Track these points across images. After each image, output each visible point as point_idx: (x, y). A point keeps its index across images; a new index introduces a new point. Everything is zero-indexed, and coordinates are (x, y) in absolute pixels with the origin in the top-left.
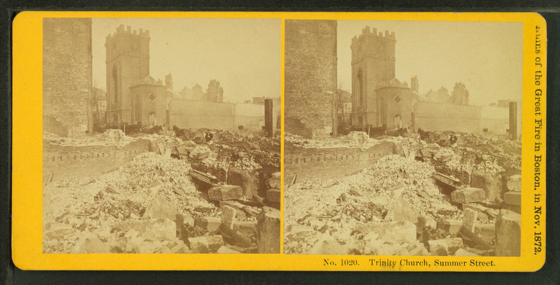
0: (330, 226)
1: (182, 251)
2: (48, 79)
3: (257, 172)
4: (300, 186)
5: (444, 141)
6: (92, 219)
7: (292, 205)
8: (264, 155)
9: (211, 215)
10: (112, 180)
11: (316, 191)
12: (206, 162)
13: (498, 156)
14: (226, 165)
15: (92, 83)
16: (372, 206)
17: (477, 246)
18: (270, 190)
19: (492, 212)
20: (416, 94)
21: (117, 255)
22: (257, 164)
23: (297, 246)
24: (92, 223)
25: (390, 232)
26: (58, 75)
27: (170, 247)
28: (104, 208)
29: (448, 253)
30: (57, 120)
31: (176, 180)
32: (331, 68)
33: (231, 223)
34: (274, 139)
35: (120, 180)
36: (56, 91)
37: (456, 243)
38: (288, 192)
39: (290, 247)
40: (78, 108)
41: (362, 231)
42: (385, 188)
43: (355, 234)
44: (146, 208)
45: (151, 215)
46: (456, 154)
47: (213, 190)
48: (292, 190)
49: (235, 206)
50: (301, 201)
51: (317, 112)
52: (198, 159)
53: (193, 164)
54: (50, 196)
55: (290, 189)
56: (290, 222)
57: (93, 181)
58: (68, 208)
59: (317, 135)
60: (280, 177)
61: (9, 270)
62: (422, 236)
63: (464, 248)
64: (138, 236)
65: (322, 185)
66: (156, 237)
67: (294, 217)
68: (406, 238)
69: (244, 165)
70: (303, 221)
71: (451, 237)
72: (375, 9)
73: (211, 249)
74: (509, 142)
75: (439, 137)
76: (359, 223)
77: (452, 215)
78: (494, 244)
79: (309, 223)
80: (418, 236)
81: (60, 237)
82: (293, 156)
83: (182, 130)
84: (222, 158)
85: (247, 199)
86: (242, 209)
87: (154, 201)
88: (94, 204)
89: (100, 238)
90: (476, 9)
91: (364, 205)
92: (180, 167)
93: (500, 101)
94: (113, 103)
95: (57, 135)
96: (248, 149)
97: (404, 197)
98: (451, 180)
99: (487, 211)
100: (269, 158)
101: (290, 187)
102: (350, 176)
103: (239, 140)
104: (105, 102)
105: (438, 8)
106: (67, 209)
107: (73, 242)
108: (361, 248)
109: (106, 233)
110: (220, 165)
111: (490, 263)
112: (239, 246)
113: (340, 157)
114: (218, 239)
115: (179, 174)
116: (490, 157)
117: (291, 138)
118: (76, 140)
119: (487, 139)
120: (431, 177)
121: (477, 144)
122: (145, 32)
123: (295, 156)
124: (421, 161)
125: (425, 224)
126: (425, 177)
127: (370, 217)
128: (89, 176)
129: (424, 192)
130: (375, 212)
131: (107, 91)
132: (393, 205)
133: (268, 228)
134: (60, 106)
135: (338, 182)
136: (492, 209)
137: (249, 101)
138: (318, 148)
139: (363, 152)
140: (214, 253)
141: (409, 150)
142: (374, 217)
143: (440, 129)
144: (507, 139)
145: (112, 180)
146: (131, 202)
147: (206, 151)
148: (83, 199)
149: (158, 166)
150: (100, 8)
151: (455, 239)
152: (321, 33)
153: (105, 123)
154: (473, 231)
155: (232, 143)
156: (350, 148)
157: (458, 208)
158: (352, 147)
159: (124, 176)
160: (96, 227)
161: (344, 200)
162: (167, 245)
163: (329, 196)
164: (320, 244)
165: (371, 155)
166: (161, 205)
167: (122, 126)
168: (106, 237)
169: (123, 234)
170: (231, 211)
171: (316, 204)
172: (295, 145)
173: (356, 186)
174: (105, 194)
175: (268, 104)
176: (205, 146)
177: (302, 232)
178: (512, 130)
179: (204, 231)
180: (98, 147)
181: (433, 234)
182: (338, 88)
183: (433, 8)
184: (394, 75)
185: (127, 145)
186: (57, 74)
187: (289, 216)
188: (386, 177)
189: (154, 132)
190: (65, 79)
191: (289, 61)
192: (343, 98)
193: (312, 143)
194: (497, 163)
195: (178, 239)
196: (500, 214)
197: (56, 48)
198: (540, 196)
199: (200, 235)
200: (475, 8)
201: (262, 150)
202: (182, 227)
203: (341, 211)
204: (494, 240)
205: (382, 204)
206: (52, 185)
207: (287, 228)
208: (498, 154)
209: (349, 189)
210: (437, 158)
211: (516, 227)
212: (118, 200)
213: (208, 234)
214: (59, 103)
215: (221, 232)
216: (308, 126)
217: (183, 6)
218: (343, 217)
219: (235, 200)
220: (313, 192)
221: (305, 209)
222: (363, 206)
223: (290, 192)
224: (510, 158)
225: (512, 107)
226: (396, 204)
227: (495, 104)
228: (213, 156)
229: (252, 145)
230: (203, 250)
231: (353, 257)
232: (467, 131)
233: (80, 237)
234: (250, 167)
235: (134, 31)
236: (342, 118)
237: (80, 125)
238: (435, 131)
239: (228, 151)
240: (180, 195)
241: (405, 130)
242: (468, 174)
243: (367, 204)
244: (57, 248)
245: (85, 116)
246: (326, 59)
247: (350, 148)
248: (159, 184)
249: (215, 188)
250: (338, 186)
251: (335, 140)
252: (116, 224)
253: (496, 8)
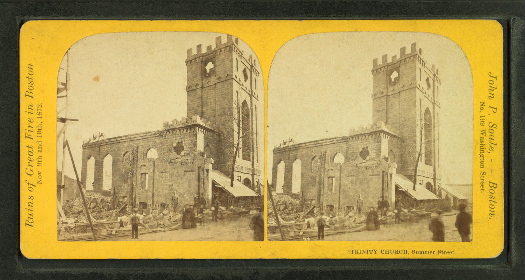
61: (16, 258)
105: (394, 15)
111: (483, 189)
150: (97, 16)
198: (28, 111)
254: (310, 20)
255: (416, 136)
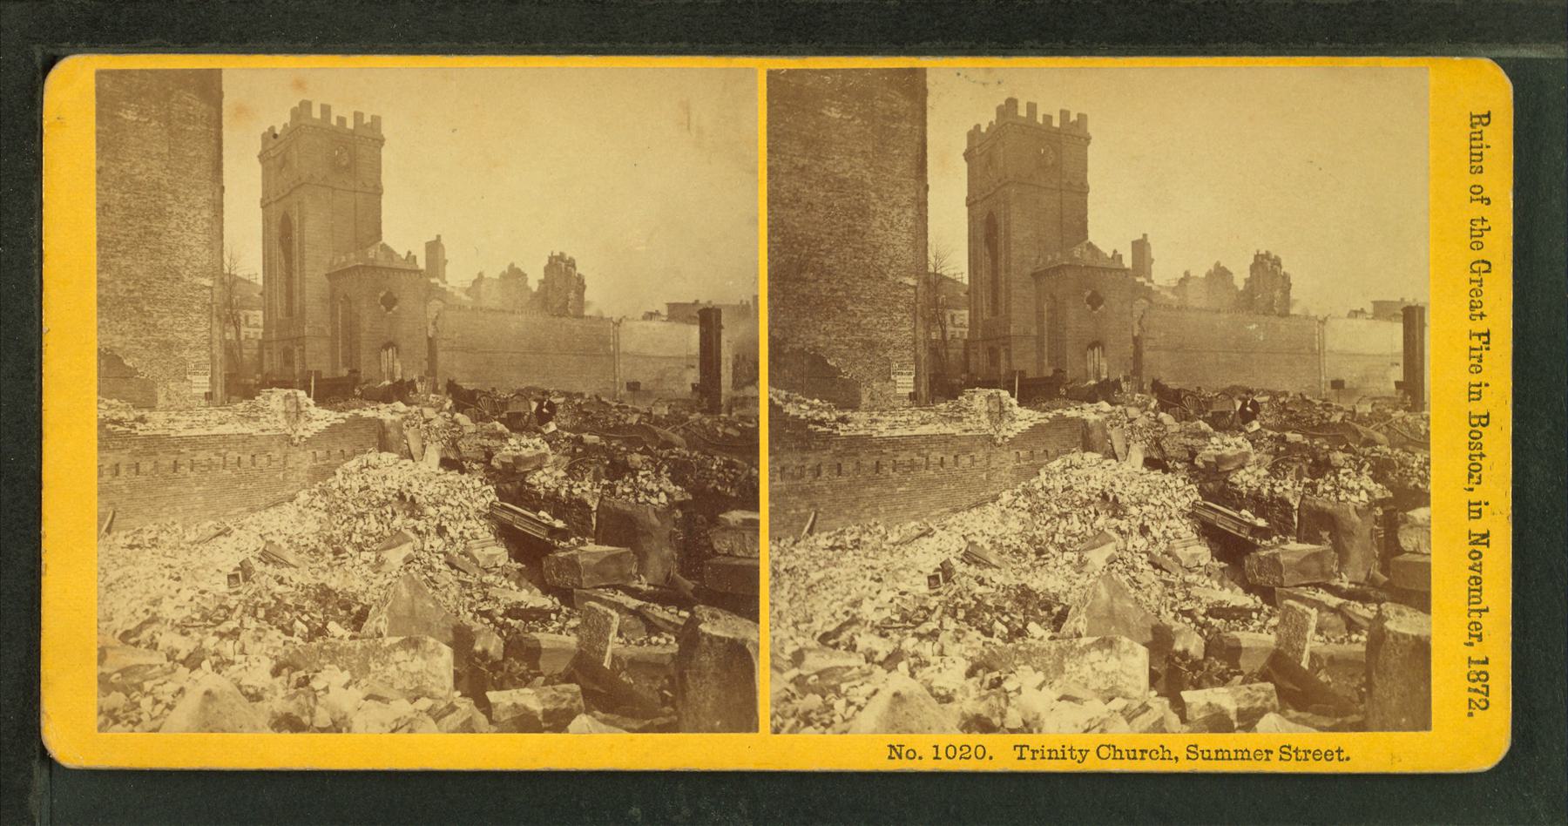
0: (213, 649)
1: (468, 727)
2: (806, 247)
3: (1378, 509)
4: (826, 542)
5: (1224, 414)
6: (222, 635)
7: (803, 593)
8: (1399, 461)
9: (551, 629)
10: (278, 530)
11: (168, 553)
12: (1239, 481)
13: (1374, 455)
14: (592, 488)
15: (222, 260)
16: (1025, 596)
17: (1315, 705)
18: (1400, 558)
19: (1362, 611)
20: (441, 285)
21: (287, 736)
22: (1379, 486)
23: (820, 707)
24: (221, 647)
25: (380, 668)
26: (128, 239)
27: (437, 716)
28: (256, 607)
29: (1236, 725)
30: (125, 361)
31: (455, 529)
32: (206, 216)
33: (1304, 650)
34: (725, 418)
35: (300, 529)
36: (828, 281)
37: (1258, 699)
38: (793, 558)
39: (800, 711)
40: (183, 331)
41: (997, 665)
42: (1062, 545)
43: (980, 672)
44: (371, 607)
45: (383, 626)
46: (1256, 450)
47: (557, 558)
48: (804, 551)
49: (616, 604)
50: (129, 580)
51: (170, 336)
52: (1217, 473)
53: (500, 485)
54: (807, 576)
55: (799, 548)
56: (801, 641)
57: (225, 532)
58: (154, 605)
59: (169, 399)
60: (1429, 521)
62: (1163, 678)
63: (1281, 712)
64: (346, 686)
65: (887, 538)
66: (1094, 687)
67: (809, 628)
68: (1119, 683)
69: (641, 489)
70: (135, 635)
71: (1243, 682)
72: (1047, 48)
73: (549, 722)
74: (1403, 418)
75: (1209, 403)
76: (990, 643)
77: (1246, 621)
78: (1362, 701)
79: (154, 641)
80: (1154, 678)
81: (134, 685)
82: (107, 457)
83: (472, 394)
84: (581, 472)
85: (649, 585)
86: (1337, 611)
87: (392, 589)
88: (927, 596)
89: (244, 690)
90: (1325, 48)
91: (1004, 594)
92: (1168, 493)
93: (1376, 304)
94: (280, 316)
95: (124, 405)
96: (1355, 443)
97: (1114, 571)
98: (1245, 523)
99: (642, 610)
100: (1413, 468)
101: (798, 544)
102: (966, 513)
103: (628, 422)
104: (260, 313)
105: (1220, 44)
106: (153, 609)
107: (168, 699)
108: (997, 712)
109: (259, 674)
110: (1278, 490)
112: (1318, 712)
113: (235, 461)
114: (569, 696)
115: (1165, 515)
116: (1351, 458)
117: (800, 409)
118: (179, 418)
119: (1341, 409)
120: (485, 516)
121: (1316, 423)
122: (370, 121)
123: (812, 460)
124: (1160, 471)
125: (1172, 646)
126: (1173, 515)
127: (1020, 626)
128: (212, 517)
129: (1169, 556)
130: (334, 612)
131: (264, 282)
132: (1084, 592)
133: (1392, 661)
134: (135, 325)
135: (931, 530)
136: (1358, 604)
137: (1362, 311)
138: (173, 434)
139: (1000, 446)
140: (1248, 732)
141: (1128, 439)
142: (1032, 626)
143: (1214, 382)
144: (1396, 409)
145: (278, 530)
146: (1031, 591)
147: (536, 452)
148: (898, 581)
149: (1106, 490)
151: (1255, 686)
152: (885, 117)
153: (257, 372)
154: (1305, 664)
155: (1313, 427)
156: (964, 434)
157: (560, 601)
158: (267, 433)
159: (310, 517)
160: (231, 659)
161: (246, 579)
162: (1123, 712)
163: (204, 567)
164: (883, 701)
165: (319, 453)
166: (1112, 601)
167: (1008, 381)
168: (259, 685)
169: (306, 678)
170: (1303, 616)
171: (870, 589)
172: (811, 426)
173: (278, 540)
174: (258, 567)
175: (709, 319)
176: (534, 438)
177: (831, 669)
178: (1412, 388)
179: (1229, 673)
180: (240, 437)
181: (1194, 673)
182: (931, 269)
183: (1208, 45)
184: (379, 233)
185: (319, 434)
186: (830, 234)
187: (795, 624)
188: (362, 516)
189: (1100, 397)
190: (147, 251)
191: (795, 194)
192: (238, 297)
193: (858, 423)
194: (1371, 476)
195: (1154, 693)
196: (1380, 618)
197: (828, 162)
199: (521, 683)
200: (1324, 45)
201: (691, 447)
202: (1170, 659)
203: (240, 608)
204: (1364, 690)
205: (1051, 591)
206: (112, 543)
207: (789, 658)
208: (1373, 451)
209: (960, 550)
210: (1205, 462)
211: (1421, 649)
212: (294, 584)
213: (541, 679)
214: (131, 314)
215: (578, 674)
216: (848, 373)
217: (518, 41)
218: (945, 627)
219: (1317, 586)
220: (862, 557)
221: (840, 603)
222: (1001, 594)
223: (798, 557)
224: (1407, 461)
225: (1412, 318)
226: (1091, 589)
227: (1362, 311)
228: (1259, 463)
229: (1367, 433)
230: (525, 722)
231: (976, 738)
232: (1287, 387)
233: (187, 685)
234: (1359, 494)
235: (338, 118)
236: (237, 351)
237: (893, 377)
238: (494, 389)
239: (1300, 449)
240: (1167, 571)
241: (412, 385)
242: (590, 508)
243: (1012, 591)
244: (123, 715)
245: (908, 352)
246: (194, 191)
247: (964, 434)
248: (1111, 540)
249: (561, 555)
250: (932, 541)
251: (922, 413)
252: (287, 651)
253: (1381, 44)
254: (163, 53)
255: (757, 208)
